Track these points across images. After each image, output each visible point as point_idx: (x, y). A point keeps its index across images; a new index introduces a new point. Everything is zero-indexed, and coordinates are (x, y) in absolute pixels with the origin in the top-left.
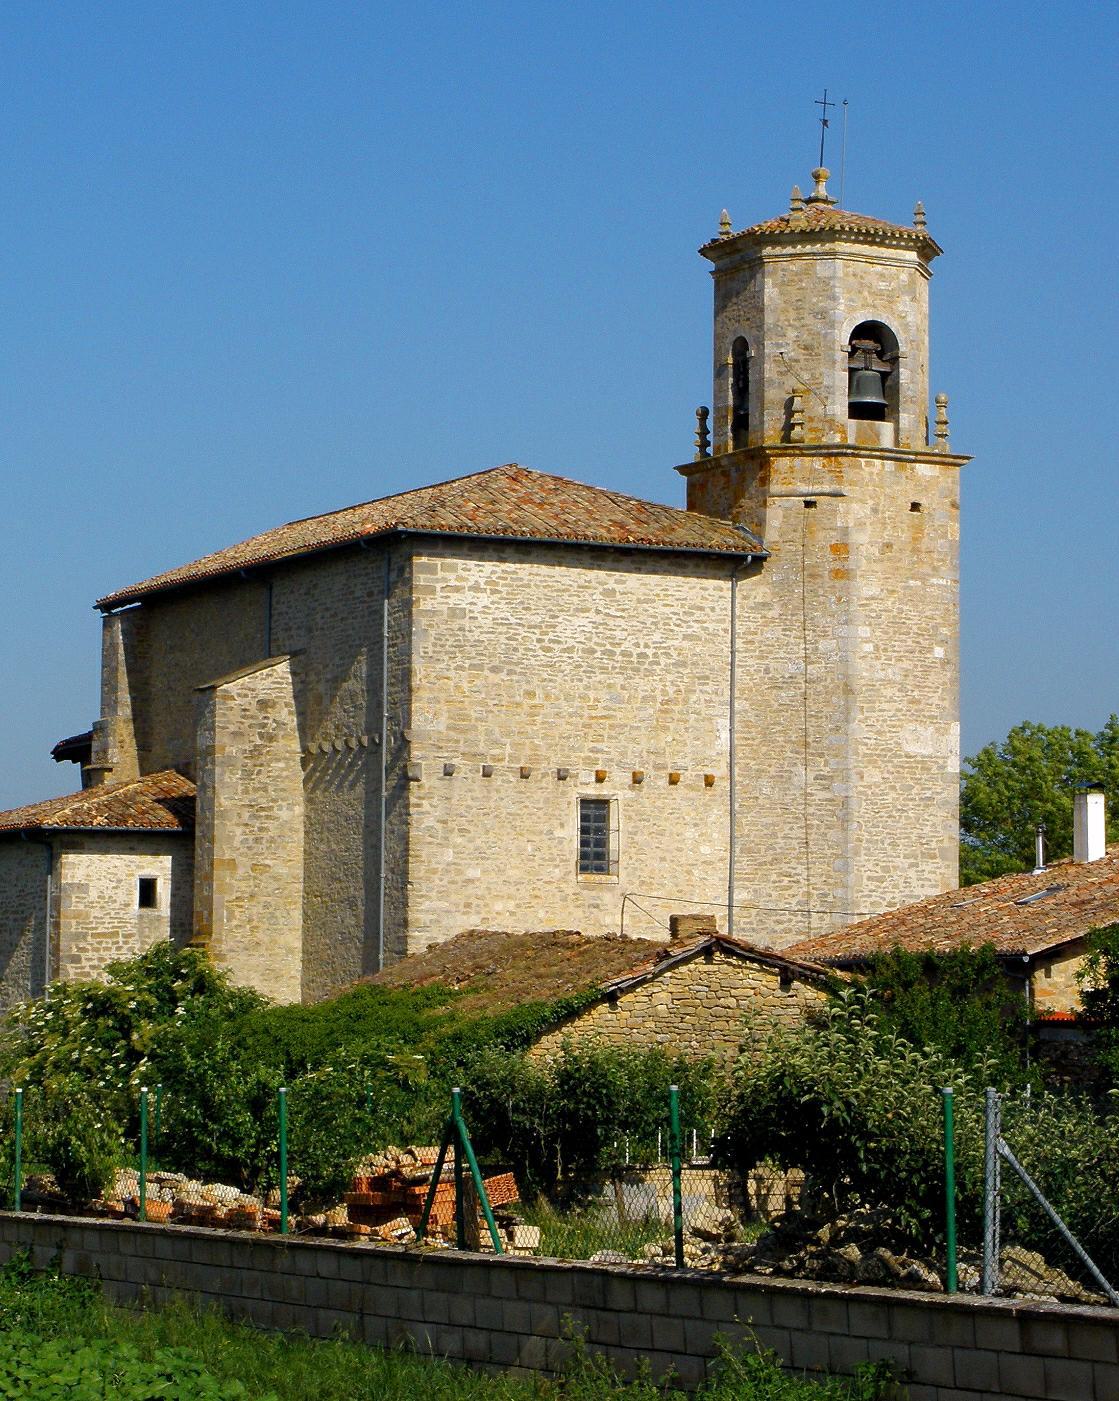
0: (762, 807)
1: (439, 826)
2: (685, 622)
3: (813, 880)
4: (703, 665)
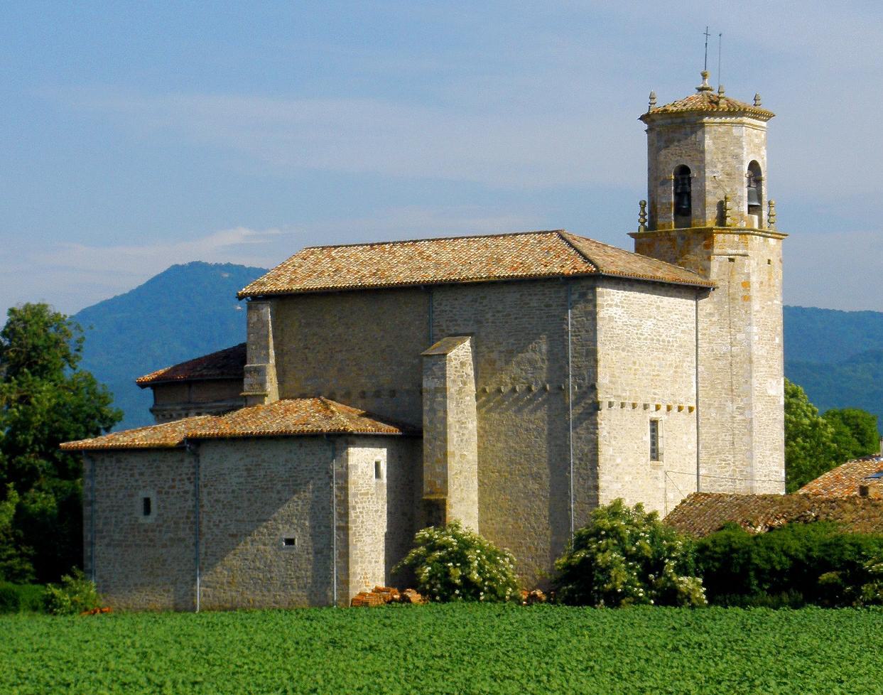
0: (712, 424)
3: (737, 463)
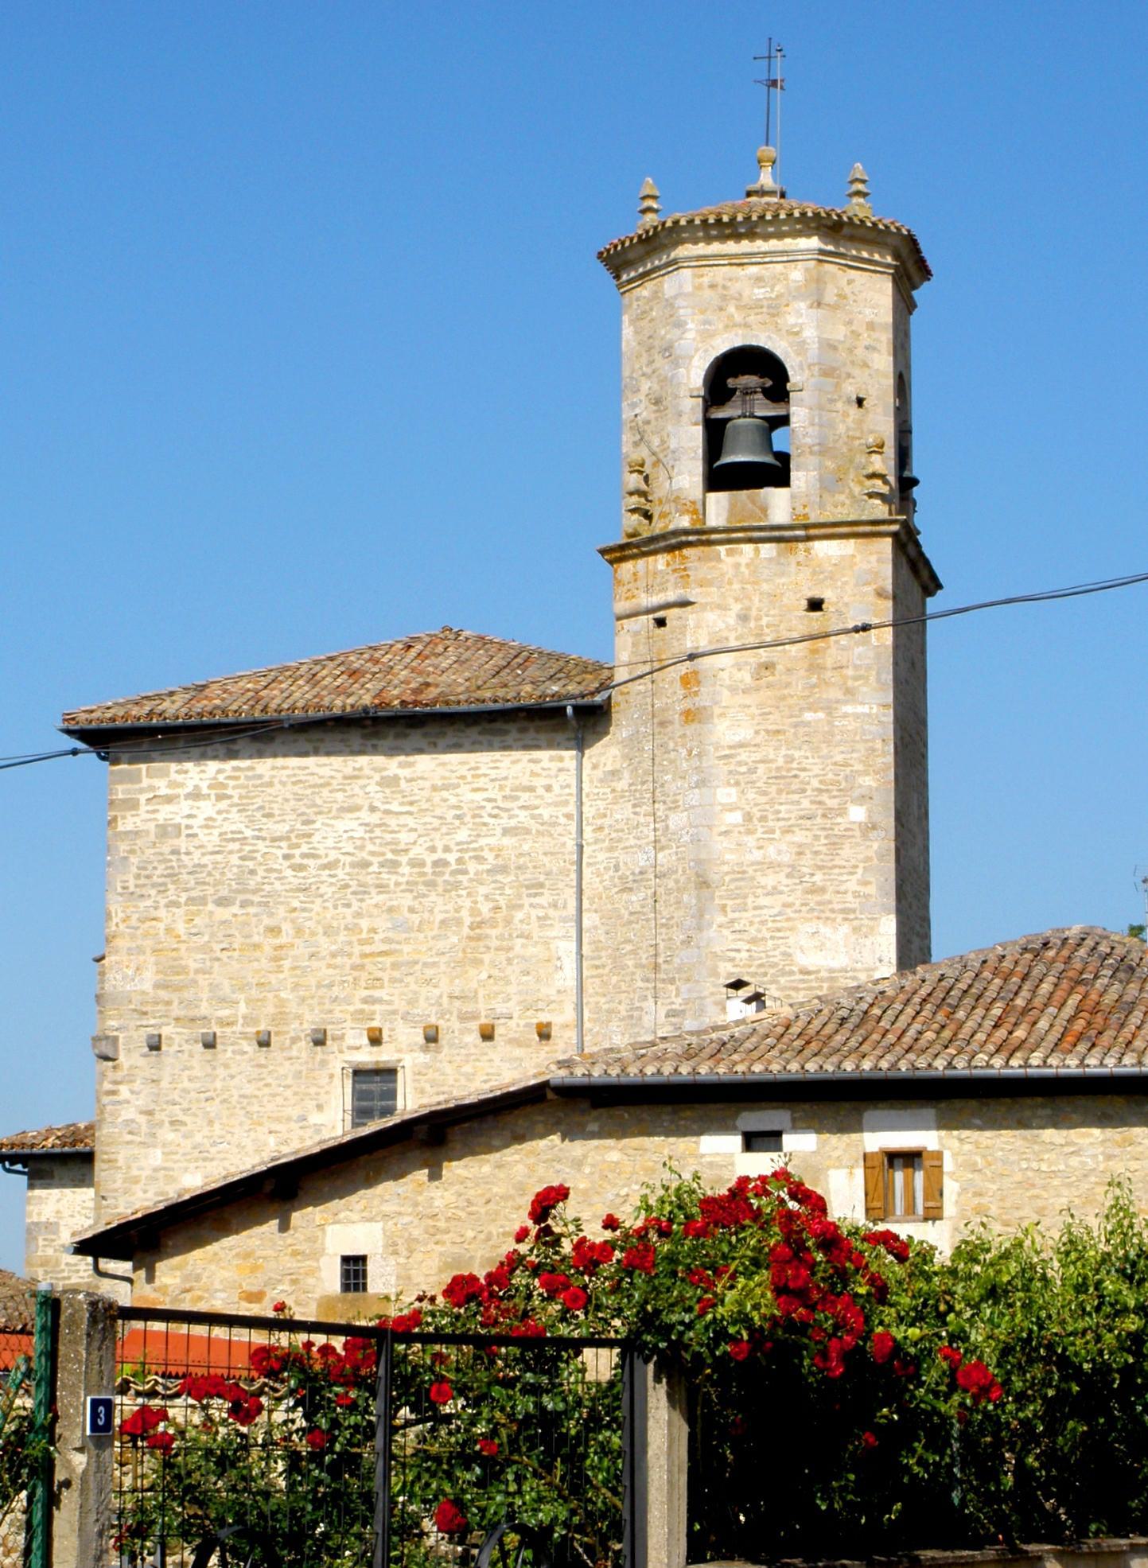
1: (142, 1119)
2: (507, 810)
4: (535, 867)
